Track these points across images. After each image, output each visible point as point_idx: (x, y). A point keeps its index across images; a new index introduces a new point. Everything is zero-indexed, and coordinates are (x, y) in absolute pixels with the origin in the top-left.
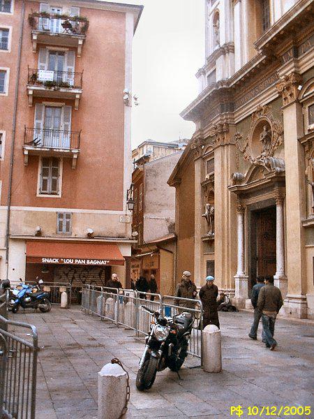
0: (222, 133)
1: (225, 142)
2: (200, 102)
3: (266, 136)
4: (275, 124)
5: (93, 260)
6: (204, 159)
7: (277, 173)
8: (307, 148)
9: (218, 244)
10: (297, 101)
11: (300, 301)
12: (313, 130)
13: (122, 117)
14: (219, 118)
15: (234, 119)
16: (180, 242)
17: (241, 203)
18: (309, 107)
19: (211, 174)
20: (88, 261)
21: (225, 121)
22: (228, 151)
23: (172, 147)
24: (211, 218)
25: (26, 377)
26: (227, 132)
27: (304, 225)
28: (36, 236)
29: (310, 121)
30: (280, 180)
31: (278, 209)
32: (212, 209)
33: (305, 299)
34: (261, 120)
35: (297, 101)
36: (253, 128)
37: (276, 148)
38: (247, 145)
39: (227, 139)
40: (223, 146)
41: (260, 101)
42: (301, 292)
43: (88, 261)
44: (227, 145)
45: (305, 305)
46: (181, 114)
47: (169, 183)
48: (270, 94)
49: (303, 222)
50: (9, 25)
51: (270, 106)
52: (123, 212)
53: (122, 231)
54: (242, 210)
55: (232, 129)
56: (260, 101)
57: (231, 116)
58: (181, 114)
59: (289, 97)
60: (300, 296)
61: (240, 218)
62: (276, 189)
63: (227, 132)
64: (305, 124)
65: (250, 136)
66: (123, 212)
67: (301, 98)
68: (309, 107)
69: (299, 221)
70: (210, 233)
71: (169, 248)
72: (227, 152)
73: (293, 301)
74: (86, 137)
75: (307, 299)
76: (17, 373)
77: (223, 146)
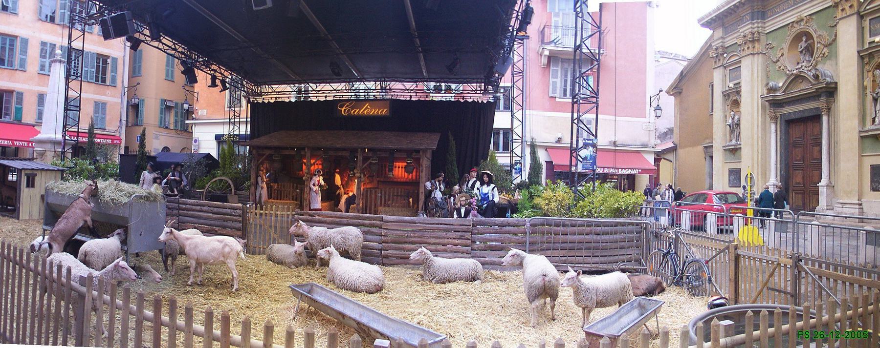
0: (753, 41)
1: (756, 51)
2: (726, 8)
3: (806, 47)
4: (820, 35)
5: (625, 169)
6: (725, 67)
7: (827, 83)
8: (866, 60)
9: (745, 152)
10: (858, 13)
11: (857, 207)
12: (878, 42)
14: (750, 26)
15: (765, 28)
16: (680, 151)
17: (774, 112)
18: (870, 20)
19: (735, 82)
20: (620, 170)
21: (756, 29)
22: (758, 60)
23: (676, 58)
24: (735, 128)
25: (205, 208)
27: (862, 135)
28: (556, 142)
29: (870, 34)
30: (831, 91)
31: (825, 119)
32: (737, 117)
33: (861, 205)
34: (804, 30)
35: (858, 13)
36: (790, 39)
37: (820, 59)
38: (782, 55)
39: (758, 47)
40: (754, 54)
41: (801, 11)
43: (620, 170)
44: (758, 54)
45: (861, 210)
46: (699, 21)
47: (216, 135)
48: (813, 6)
49: (860, 132)
50: (257, 11)
51: (814, 17)
52: (647, 120)
53: (645, 139)
54: (775, 119)
55: (763, 38)
56: (801, 11)
58: (699, 21)
59: (847, 8)
60: (857, 202)
61: (773, 126)
62: (823, 99)
63: (758, 40)
64: (865, 36)
65: (786, 46)
66: (647, 120)
67: (862, 10)
68: (870, 20)
69: (857, 131)
70: (734, 142)
71: (668, 157)
72: (758, 61)
73: (847, 206)
75: (863, 205)
76: (216, 210)
77: (754, 54)
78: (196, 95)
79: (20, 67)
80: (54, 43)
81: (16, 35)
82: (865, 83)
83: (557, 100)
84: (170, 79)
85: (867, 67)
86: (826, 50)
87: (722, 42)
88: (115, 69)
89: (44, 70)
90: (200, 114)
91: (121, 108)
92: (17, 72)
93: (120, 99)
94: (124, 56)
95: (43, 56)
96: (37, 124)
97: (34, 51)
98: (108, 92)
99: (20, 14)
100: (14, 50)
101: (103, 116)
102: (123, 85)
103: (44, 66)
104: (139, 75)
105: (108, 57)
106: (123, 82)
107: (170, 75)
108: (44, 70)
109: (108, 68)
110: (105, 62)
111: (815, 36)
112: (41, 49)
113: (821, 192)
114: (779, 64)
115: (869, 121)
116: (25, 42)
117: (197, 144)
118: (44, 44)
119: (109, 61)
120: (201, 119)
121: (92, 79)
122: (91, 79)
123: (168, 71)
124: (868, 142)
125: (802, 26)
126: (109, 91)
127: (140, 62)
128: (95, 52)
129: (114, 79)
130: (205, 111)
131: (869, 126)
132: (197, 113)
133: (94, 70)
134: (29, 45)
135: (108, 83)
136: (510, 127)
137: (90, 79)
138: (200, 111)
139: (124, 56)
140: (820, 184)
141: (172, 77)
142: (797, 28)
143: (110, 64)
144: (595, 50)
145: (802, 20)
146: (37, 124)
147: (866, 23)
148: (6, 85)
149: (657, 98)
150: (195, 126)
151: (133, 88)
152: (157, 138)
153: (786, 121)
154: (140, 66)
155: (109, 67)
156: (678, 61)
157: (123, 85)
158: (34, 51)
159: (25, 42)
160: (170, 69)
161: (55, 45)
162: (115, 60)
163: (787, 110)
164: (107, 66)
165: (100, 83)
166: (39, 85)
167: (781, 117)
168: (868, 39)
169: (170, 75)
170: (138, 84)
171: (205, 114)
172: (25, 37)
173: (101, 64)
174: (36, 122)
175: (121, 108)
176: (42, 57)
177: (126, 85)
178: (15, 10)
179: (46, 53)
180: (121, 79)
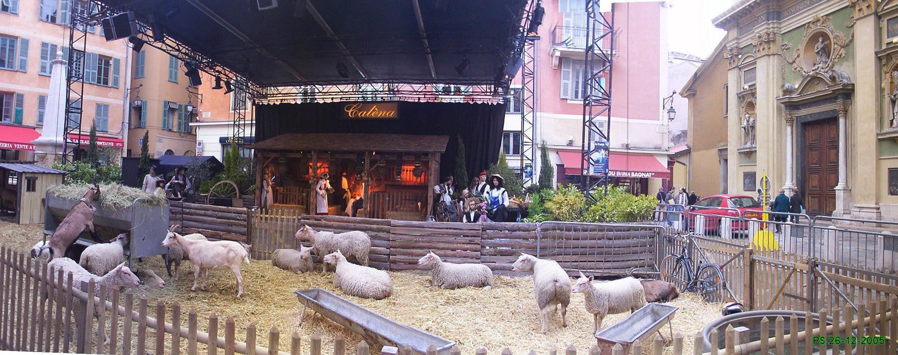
0: (768, 42)
1: (771, 52)
2: (741, 8)
4: (837, 36)
5: (638, 172)
6: (740, 69)
7: (844, 85)
8: (884, 61)
9: (760, 155)
10: (876, 13)
11: (875, 211)
12: (896, 43)
13: (658, 19)
14: (765, 26)
15: (780, 28)
16: (694, 154)
17: (790, 115)
18: (888, 20)
19: (750, 84)
20: (633, 173)
21: (771, 30)
22: (773, 61)
24: (750, 130)
26: (774, 41)
27: (879, 137)
28: (568, 145)
29: (888, 35)
30: (848, 93)
31: (842, 121)
32: (752, 119)
33: (878, 209)
35: (876, 13)
36: (806, 40)
37: (837, 60)
38: (798, 56)
39: (774, 48)
40: (769, 55)
41: (817, 12)
42: (874, 202)
43: (633, 173)
44: (773, 55)
45: (879, 214)
46: (714, 21)
48: (830, 6)
49: (878, 135)
51: (830, 17)
52: (660, 122)
54: (790, 121)
55: (779, 39)
56: (817, 12)
57: (778, 26)
58: (714, 21)
59: (864, 8)
60: (874, 206)
61: (789, 129)
62: (840, 101)
63: (774, 41)
64: (883, 36)
65: (802, 47)
67: (880, 10)
68: (888, 20)
69: (875, 134)
70: (749, 145)
71: (682, 160)
72: (773, 62)
73: (865, 210)
74: (621, 40)
75: (881, 209)
77: (769, 55)
78: (200, 97)
79: (21, 68)
80: (55, 44)
81: (16, 35)
82: (883, 85)
83: (569, 102)
84: (173, 80)
85: (885, 69)
86: (843, 51)
87: (737, 43)
88: (117, 70)
89: (45, 72)
90: (204, 116)
91: (124, 110)
92: (18, 73)
93: (123, 101)
94: (127, 57)
95: (44, 57)
96: (38, 126)
97: (34, 52)
98: (110, 93)
99: (21, 15)
100: (15, 51)
101: (105, 118)
102: (125, 86)
103: (45, 68)
104: (142, 76)
105: (111, 58)
106: (125, 83)
107: (173, 76)
108: (45, 72)
109: (111, 69)
110: (107, 63)
111: (831, 37)
112: (42, 50)
113: (838, 195)
114: (795, 65)
115: (886, 123)
116: (26, 43)
117: (201, 146)
118: (44, 45)
119: (111, 62)
120: (205, 121)
121: (94, 81)
122: (93, 80)
123: (171, 72)
124: (886, 145)
125: (818, 27)
126: (112, 92)
127: (143, 63)
128: (97, 53)
129: (116, 81)
130: (210, 113)
131: (886, 129)
132: (201, 115)
133: (96, 72)
134: (30, 46)
135: (110, 84)
136: (520, 130)
137: (92, 80)
138: (204, 113)
139: (127, 57)
140: (837, 188)
141: (176, 78)
142: (814, 29)
143: (112, 65)
144: (607, 51)
145: (818, 20)
146: (38, 126)
147: (884, 24)
148: (6, 87)
149: (670, 100)
150: (199, 128)
151: (135, 89)
152: (160, 141)
153: (802, 123)
154: (143, 68)
155: (111, 69)
156: (692, 62)
157: (125, 86)
158: (34, 52)
159: (26, 43)
160: (174, 71)
161: (56, 46)
162: (117, 61)
163: (803, 112)
164: (109, 67)
165: (102, 84)
166: (40, 87)
167: (797, 120)
168: (886, 40)
169: (173, 76)
170: (141, 85)
171: (210, 116)
172: (26, 38)
173: (103, 66)
174: (37, 125)
175: (124, 110)
176: (42, 58)
177: (129, 86)
178: (16, 10)
179: (47, 54)
180: (124, 81)
